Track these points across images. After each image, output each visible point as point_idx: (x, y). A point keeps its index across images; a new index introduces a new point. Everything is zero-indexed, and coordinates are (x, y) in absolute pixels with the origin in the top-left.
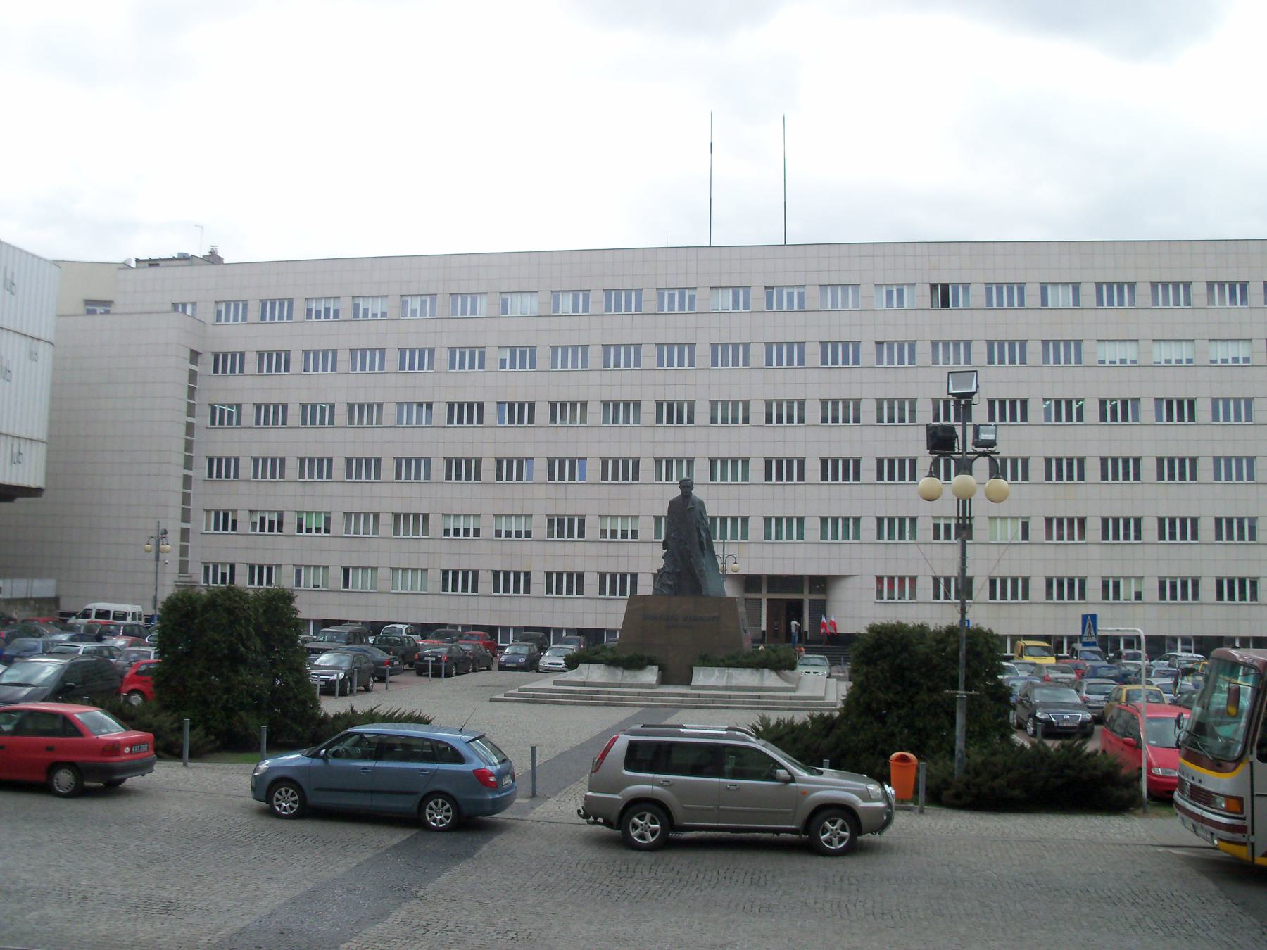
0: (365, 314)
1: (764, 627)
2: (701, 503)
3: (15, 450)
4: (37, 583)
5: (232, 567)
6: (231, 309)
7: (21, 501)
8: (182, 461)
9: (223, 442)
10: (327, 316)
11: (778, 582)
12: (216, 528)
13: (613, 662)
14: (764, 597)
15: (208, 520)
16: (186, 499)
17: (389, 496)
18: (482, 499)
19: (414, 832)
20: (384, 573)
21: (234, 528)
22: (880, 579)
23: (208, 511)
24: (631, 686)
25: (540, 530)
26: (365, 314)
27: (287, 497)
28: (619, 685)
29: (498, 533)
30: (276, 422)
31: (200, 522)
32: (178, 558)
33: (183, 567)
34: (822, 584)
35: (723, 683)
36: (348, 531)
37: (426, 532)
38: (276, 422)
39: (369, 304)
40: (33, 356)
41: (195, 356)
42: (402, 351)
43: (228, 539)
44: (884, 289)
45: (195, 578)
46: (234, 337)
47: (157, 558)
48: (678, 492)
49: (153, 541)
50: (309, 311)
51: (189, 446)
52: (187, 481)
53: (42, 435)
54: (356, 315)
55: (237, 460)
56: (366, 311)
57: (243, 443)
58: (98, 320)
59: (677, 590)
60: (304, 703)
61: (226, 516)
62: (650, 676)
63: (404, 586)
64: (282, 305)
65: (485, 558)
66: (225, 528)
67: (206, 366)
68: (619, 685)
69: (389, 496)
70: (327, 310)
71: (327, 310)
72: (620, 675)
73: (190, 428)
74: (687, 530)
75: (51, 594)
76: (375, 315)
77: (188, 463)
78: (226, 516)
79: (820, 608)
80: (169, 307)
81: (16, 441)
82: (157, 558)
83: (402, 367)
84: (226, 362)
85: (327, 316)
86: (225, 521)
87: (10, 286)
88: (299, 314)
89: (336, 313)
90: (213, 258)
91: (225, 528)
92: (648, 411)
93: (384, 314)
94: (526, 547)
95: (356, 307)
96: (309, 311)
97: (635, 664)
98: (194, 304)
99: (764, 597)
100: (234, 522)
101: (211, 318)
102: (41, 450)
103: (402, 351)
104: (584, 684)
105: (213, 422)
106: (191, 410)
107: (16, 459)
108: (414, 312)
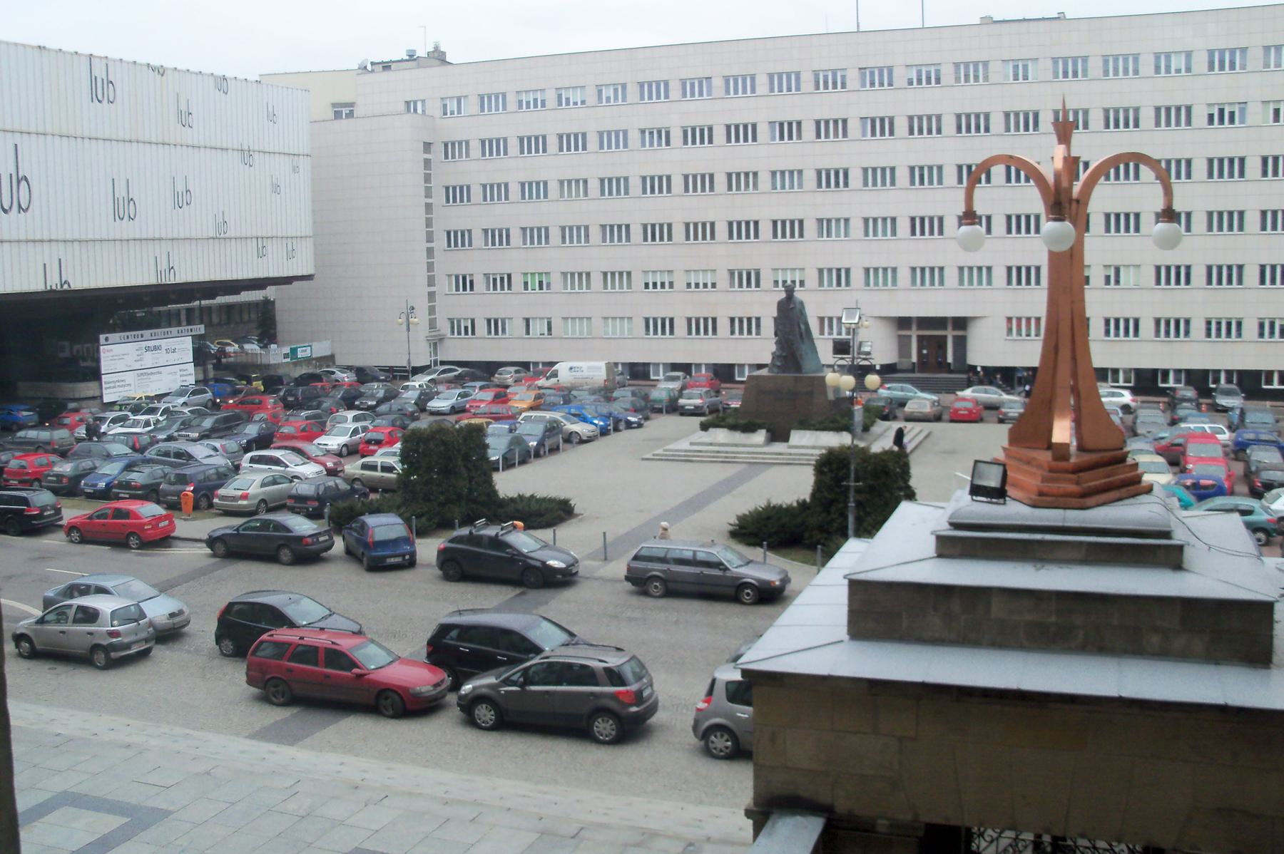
0: (568, 103)
1: (914, 359)
2: (802, 303)
3: (290, 248)
4: (316, 345)
5: (473, 321)
6: (451, 106)
7: (296, 284)
8: (424, 237)
9: (457, 217)
10: (536, 106)
11: (925, 322)
12: (457, 289)
13: (733, 428)
14: (914, 333)
15: (450, 284)
16: (430, 267)
17: (598, 257)
18: (675, 257)
19: (518, 591)
20: (597, 322)
21: (472, 289)
22: (1009, 320)
23: (450, 276)
24: (744, 446)
25: (723, 282)
26: (568, 103)
27: (513, 260)
28: (736, 445)
29: (689, 285)
30: (500, 199)
31: (444, 286)
32: (428, 317)
33: (432, 324)
34: (961, 323)
35: (811, 444)
36: (566, 288)
37: (629, 286)
38: (500, 199)
39: (571, 94)
40: (295, 169)
41: (427, 146)
42: (601, 134)
43: (467, 298)
44: (1011, 64)
45: (442, 332)
46: (457, 129)
47: (408, 330)
48: (783, 295)
49: (404, 317)
50: (520, 102)
51: (429, 223)
52: (430, 252)
53: (309, 231)
54: (560, 104)
55: (505, 140)
56: (568, 99)
57: (474, 217)
58: (344, 123)
59: (783, 369)
60: (488, 495)
61: (464, 278)
62: (760, 436)
63: (614, 332)
64: (497, 98)
65: (681, 307)
66: (465, 289)
67: (437, 154)
68: (736, 445)
69: (598, 257)
70: (535, 100)
71: (535, 100)
72: (738, 437)
73: (429, 207)
74: (790, 318)
75: (328, 353)
76: (575, 103)
77: (430, 238)
78: (464, 278)
79: (961, 343)
80: (402, 107)
81: (289, 241)
82: (408, 330)
83: (601, 147)
84: (452, 149)
85: (536, 106)
86: (465, 283)
87: (272, 117)
88: (512, 105)
89: (543, 104)
90: (438, 57)
91: (465, 289)
92: (810, 177)
93: (583, 102)
94: (711, 297)
95: (560, 96)
96: (520, 102)
97: (749, 428)
98: (423, 101)
99: (914, 333)
100: (472, 282)
101: (438, 112)
102: (310, 242)
103: (601, 134)
104: (711, 444)
105: (448, 201)
106: (428, 193)
107: (291, 255)
108: (608, 99)
